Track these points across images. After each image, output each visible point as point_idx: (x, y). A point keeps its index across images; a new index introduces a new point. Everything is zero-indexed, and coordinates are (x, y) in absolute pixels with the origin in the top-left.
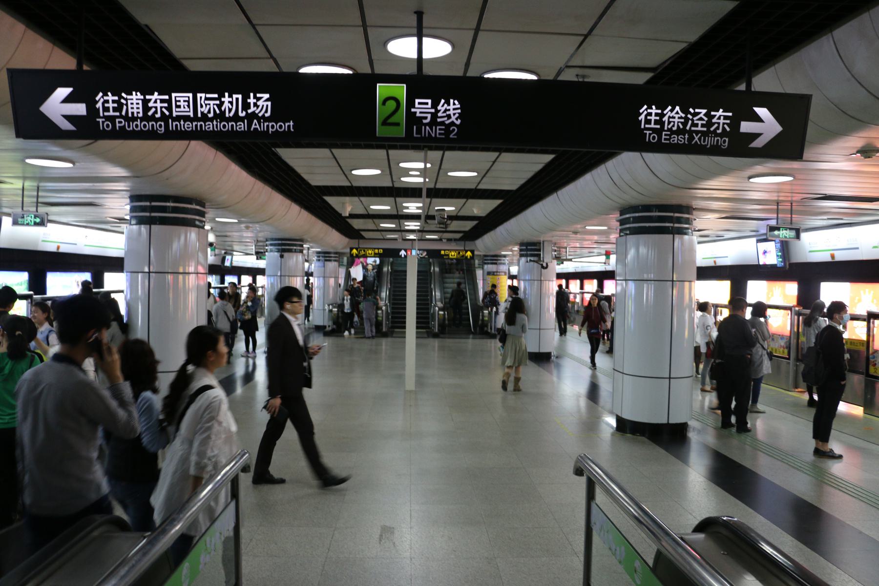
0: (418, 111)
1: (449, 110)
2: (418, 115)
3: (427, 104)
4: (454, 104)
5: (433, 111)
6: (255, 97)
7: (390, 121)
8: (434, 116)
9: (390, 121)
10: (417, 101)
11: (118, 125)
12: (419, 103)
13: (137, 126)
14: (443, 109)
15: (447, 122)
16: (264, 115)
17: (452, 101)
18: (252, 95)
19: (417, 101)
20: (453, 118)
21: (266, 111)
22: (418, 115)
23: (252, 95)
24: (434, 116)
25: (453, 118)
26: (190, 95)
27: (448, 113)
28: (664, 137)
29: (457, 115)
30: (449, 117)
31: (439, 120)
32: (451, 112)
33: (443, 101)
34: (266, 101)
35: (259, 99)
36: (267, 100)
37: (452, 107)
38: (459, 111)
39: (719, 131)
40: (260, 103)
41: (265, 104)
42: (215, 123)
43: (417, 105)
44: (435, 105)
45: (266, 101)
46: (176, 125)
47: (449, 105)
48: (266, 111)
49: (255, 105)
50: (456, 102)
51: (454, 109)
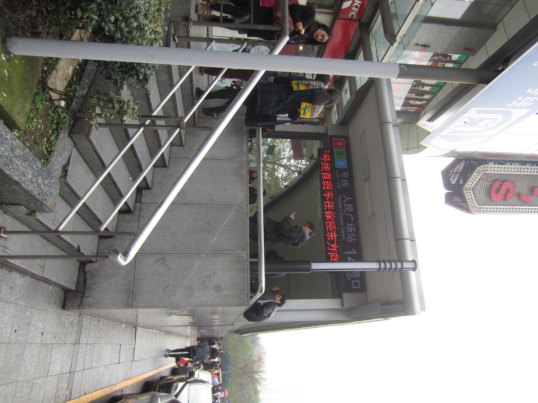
8: (343, 178)
24: (343, 178)
40: (352, 228)
44: (347, 178)
49: (350, 226)
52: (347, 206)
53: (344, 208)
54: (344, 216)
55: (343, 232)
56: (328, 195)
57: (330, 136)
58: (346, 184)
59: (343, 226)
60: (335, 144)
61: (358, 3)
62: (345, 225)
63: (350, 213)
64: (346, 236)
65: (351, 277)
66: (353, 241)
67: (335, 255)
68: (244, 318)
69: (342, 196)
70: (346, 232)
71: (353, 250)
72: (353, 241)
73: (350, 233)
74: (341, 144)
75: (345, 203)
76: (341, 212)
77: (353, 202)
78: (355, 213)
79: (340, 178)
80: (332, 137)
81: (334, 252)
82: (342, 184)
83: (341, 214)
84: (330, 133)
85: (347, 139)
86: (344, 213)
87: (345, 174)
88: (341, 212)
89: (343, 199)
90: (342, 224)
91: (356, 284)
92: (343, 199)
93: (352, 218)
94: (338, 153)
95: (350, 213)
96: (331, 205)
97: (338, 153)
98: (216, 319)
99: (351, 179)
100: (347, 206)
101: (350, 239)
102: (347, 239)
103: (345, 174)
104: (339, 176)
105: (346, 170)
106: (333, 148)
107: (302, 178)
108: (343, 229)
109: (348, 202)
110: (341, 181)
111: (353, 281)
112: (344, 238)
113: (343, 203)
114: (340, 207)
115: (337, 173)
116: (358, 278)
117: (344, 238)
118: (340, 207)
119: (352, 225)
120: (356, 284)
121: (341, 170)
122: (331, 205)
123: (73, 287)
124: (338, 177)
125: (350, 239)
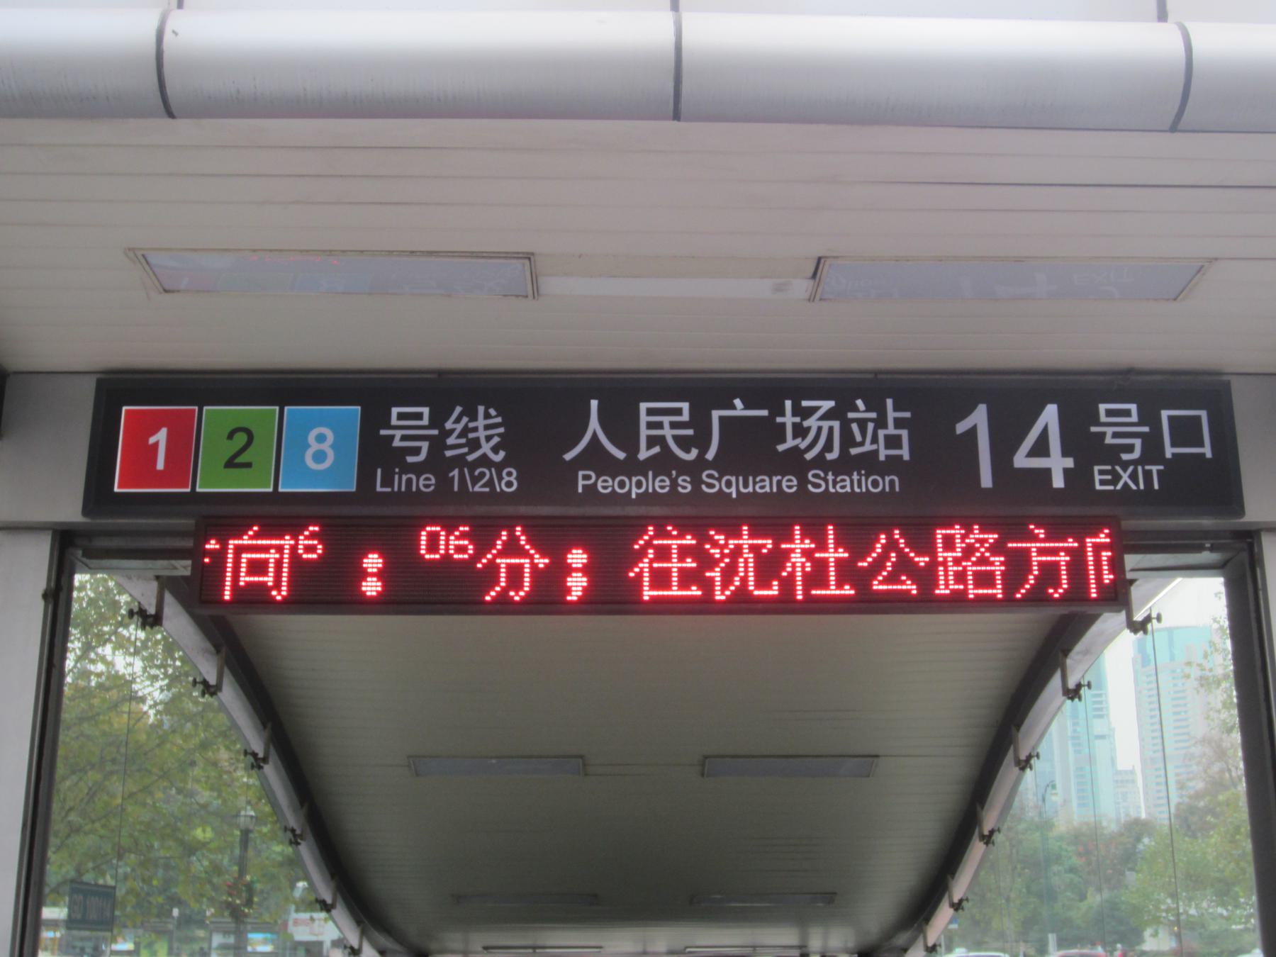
0: (1109, 431)
1: (475, 429)
2: (1109, 440)
3: (419, 416)
4: (487, 416)
5: (435, 432)
6: (798, 411)
7: (238, 460)
8: (438, 444)
9: (238, 460)
10: (1103, 407)
11: (581, 483)
12: (1110, 413)
13: (639, 485)
14: (459, 427)
15: (470, 458)
16: (821, 455)
17: (481, 409)
18: (788, 404)
19: (1103, 407)
20: (486, 448)
21: (828, 447)
22: (1109, 440)
23: (788, 404)
24: (438, 444)
26: (277, 408)
27: (471, 435)
28: (1097, 478)
29: (496, 440)
30: (474, 445)
31: (449, 453)
32: (482, 434)
33: (458, 409)
34: (825, 417)
36: (828, 416)
37: (481, 422)
38: (501, 430)
39: (832, 456)
40: (812, 423)
41: (826, 425)
42: (855, 477)
43: (1103, 418)
44: (437, 420)
45: (825, 417)
46: (746, 486)
47: (474, 418)
48: (828, 447)
49: (800, 431)
50: (492, 412)
51: (487, 427)
52: (652, 442)
53: (664, 463)
54: (724, 465)
55: (846, 485)
56: (685, 486)
57: (86, 511)
58: (486, 428)
59: (803, 482)
60: (161, 479)
62: (795, 463)
63: (700, 421)
64: (869, 463)
66: (899, 423)
67: (239, 550)
69: (580, 462)
70: (845, 465)
71: (961, 428)
72: (899, 423)
73: (847, 440)
74: (161, 437)
75: (630, 445)
76: (697, 482)
77: (622, 393)
78: (704, 390)
79: (437, 463)
80: (97, 492)
81: (1077, 557)
82: (484, 461)
83: (713, 484)
84: (70, 510)
85: (119, 389)
86: (701, 463)
87: (407, 425)
88: (697, 482)
89: (596, 458)
90: (789, 484)
91: (1186, 432)
92: (596, 458)
93: (739, 409)
94: (230, 464)
95: (700, 421)
96: (663, 554)
97: (230, 464)
99: (447, 390)
100: (652, 442)
101: (893, 442)
102: (893, 465)
103: (407, 425)
104: (418, 469)
105: (374, 421)
106: (194, 497)
107: (345, 900)
108: (820, 483)
109: (621, 425)
110: (460, 461)
111: (1169, 451)
112: (886, 483)
113: (632, 467)
114: (660, 485)
115: (400, 482)
116: (1149, 417)
117: (886, 483)
118: (660, 485)
119: (789, 419)
121: (375, 453)
122: (663, 554)
124: (426, 483)
125: (893, 442)
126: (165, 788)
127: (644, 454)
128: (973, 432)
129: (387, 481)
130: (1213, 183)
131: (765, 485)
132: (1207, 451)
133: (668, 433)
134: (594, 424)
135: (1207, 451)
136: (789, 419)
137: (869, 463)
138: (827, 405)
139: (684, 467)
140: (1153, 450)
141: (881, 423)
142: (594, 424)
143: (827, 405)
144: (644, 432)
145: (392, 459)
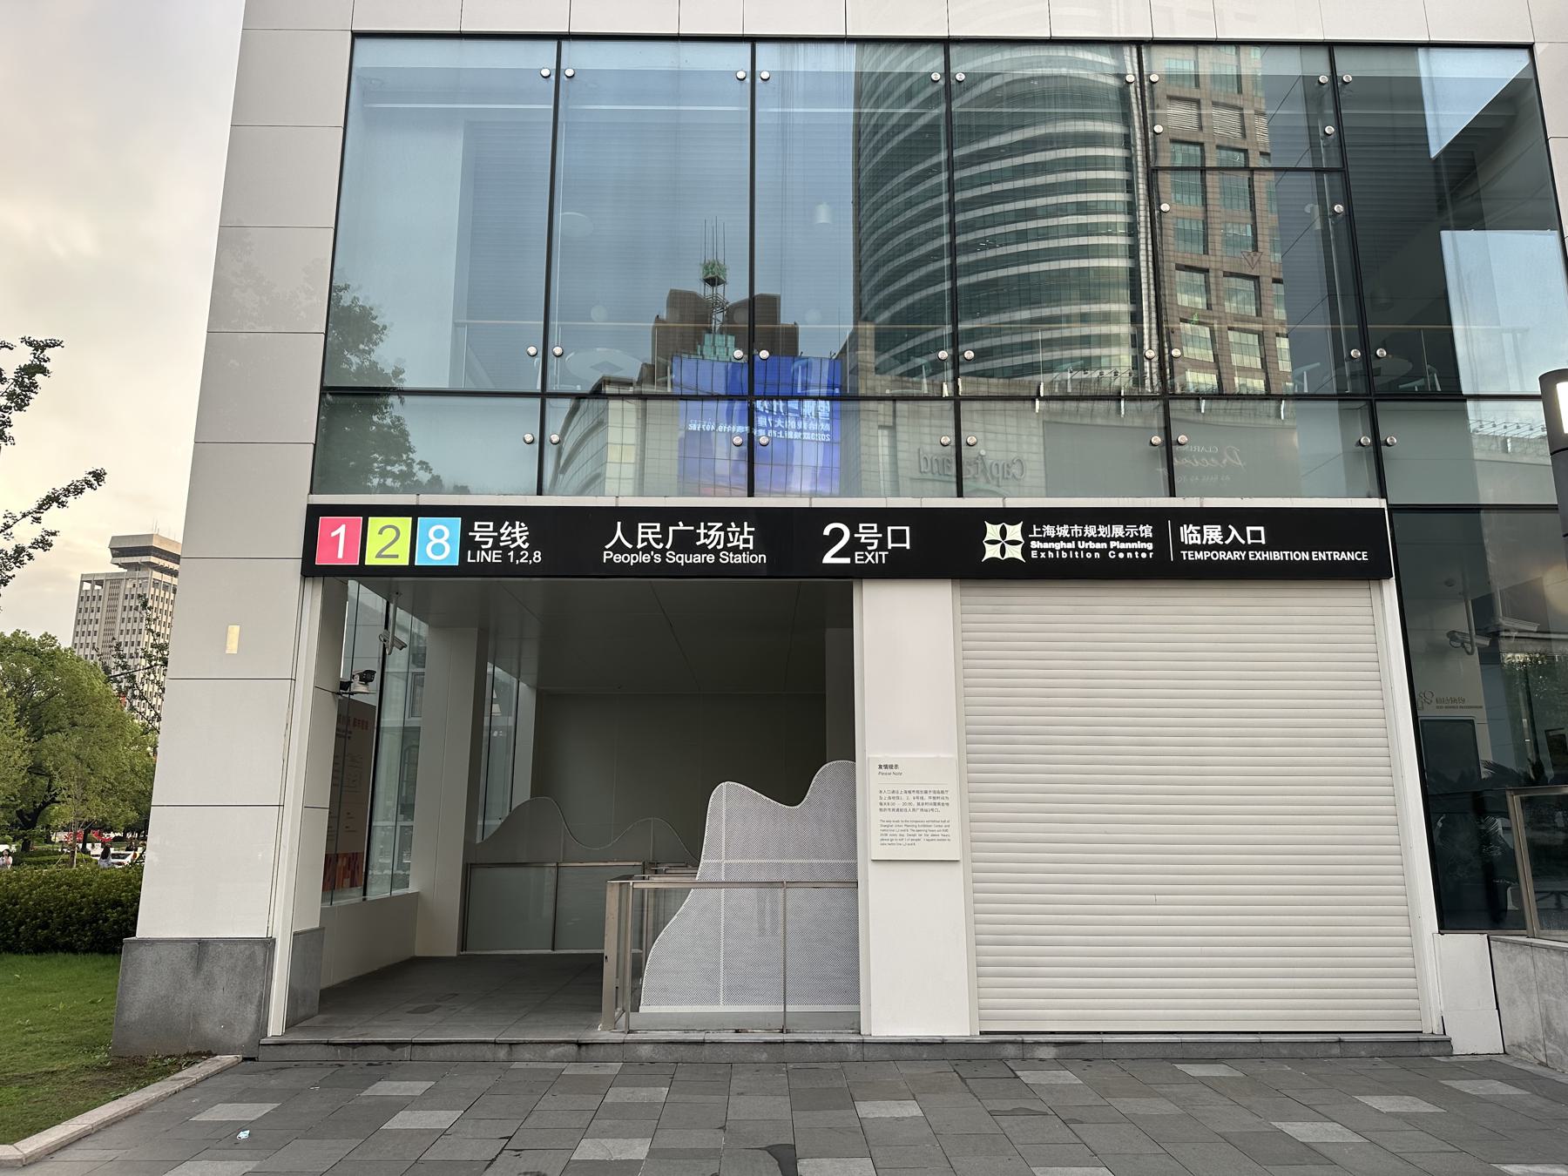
8: (497, 540)
20: (519, 542)
24: (497, 540)
25: (519, 542)
30: (514, 540)
35: (710, 528)
37: (517, 529)
40: (712, 532)
49: (707, 536)
52: (643, 540)
53: (648, 549)
61: (1563, 1079)
62: (703, 549)
63: (664, 532)
65: (878, 550)
68: (666, 296)
73: (727, 540)
75: (634, 543)
76: (664, 557)
86: (664, 551)
92: (619, 548)
93: (681, 527)
95: (664, 532)
98: (375, 460)
100: (643, 540)
101: (746, 541)
105: (466, 528)
109: (631, 535)
111: (890, 546)
113: (635, 550)
116: (882, 530)
119: (702, 531)
120: (898, 536)
121: (468, 544)
123: (1459, 247)
125: (746, 541)
126: (81, 910)
127: (640, 546)
128: (338, 536)
129: (474, 557)
130: (811, 47)
131: (698, 559)
132: (907, 546)
133: (650, 536)
134: (619, 533)
135: (907, 546)
136: (702, 531)
137: (736, 550)
138: (719, 525)
139: (656, 551)
140: (882, 545)
141: (742, 533)
142: (619, 533)
143: (719, 525)
144: (640, 536)
145: (477, 546)
